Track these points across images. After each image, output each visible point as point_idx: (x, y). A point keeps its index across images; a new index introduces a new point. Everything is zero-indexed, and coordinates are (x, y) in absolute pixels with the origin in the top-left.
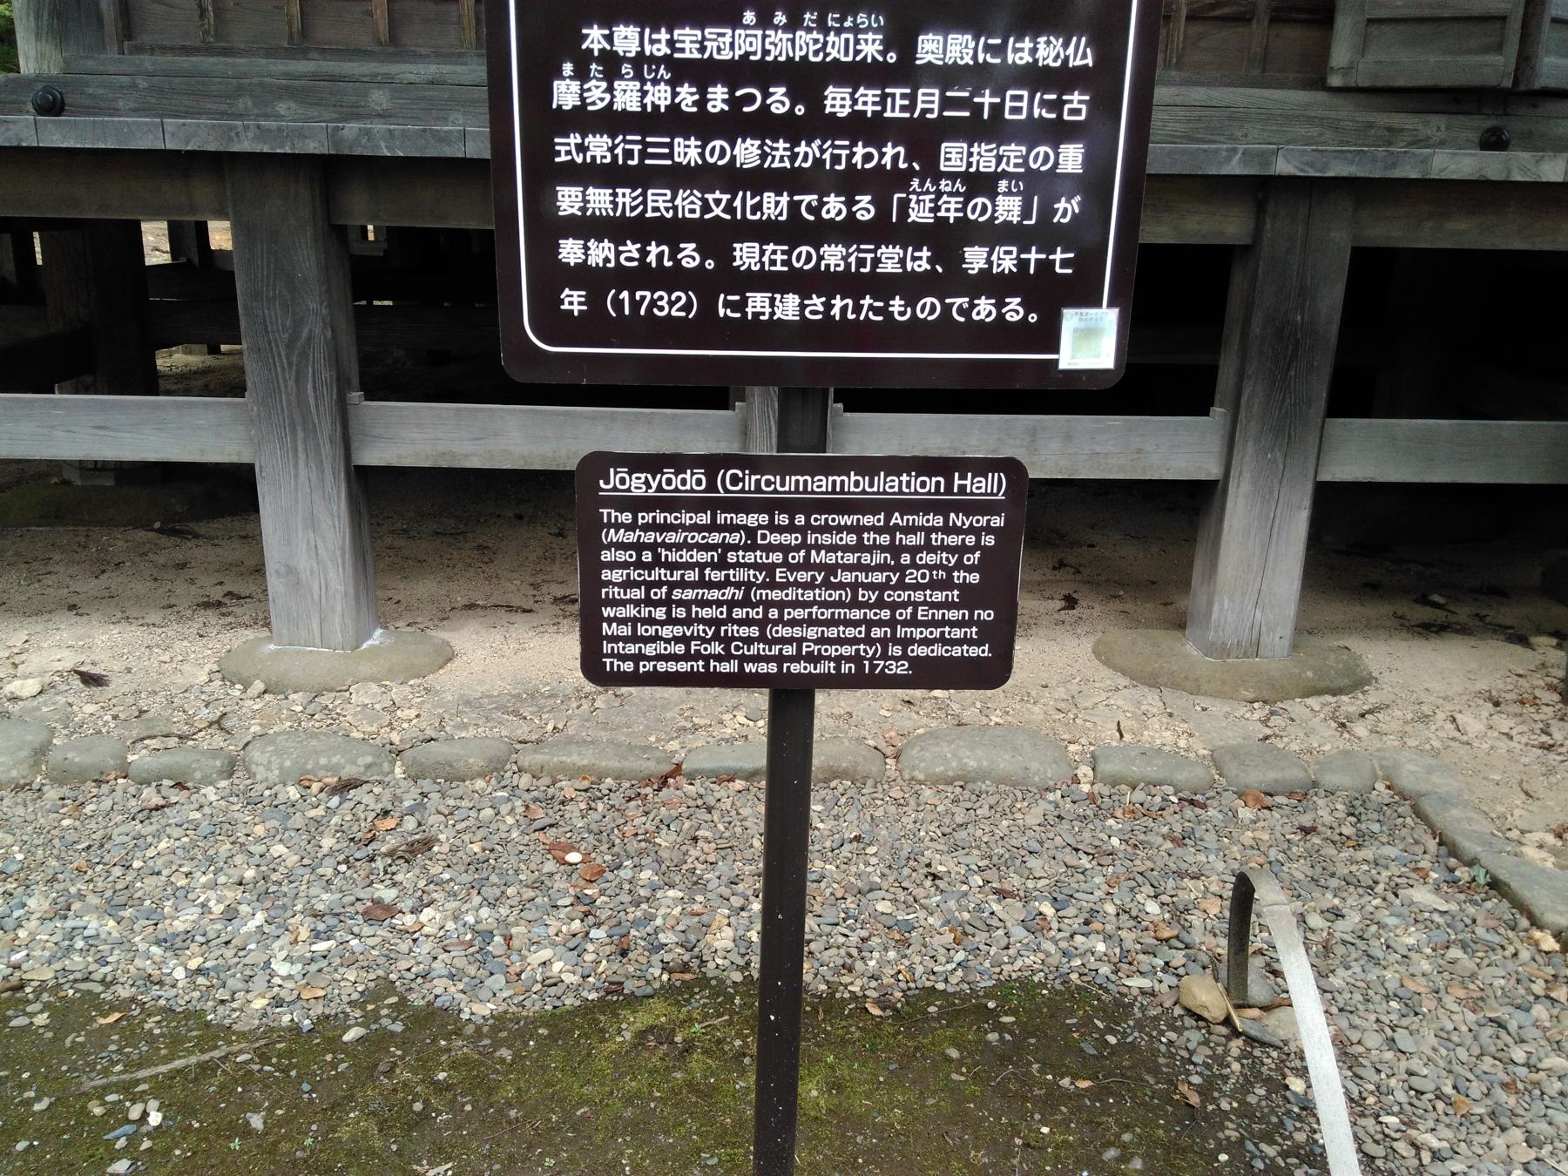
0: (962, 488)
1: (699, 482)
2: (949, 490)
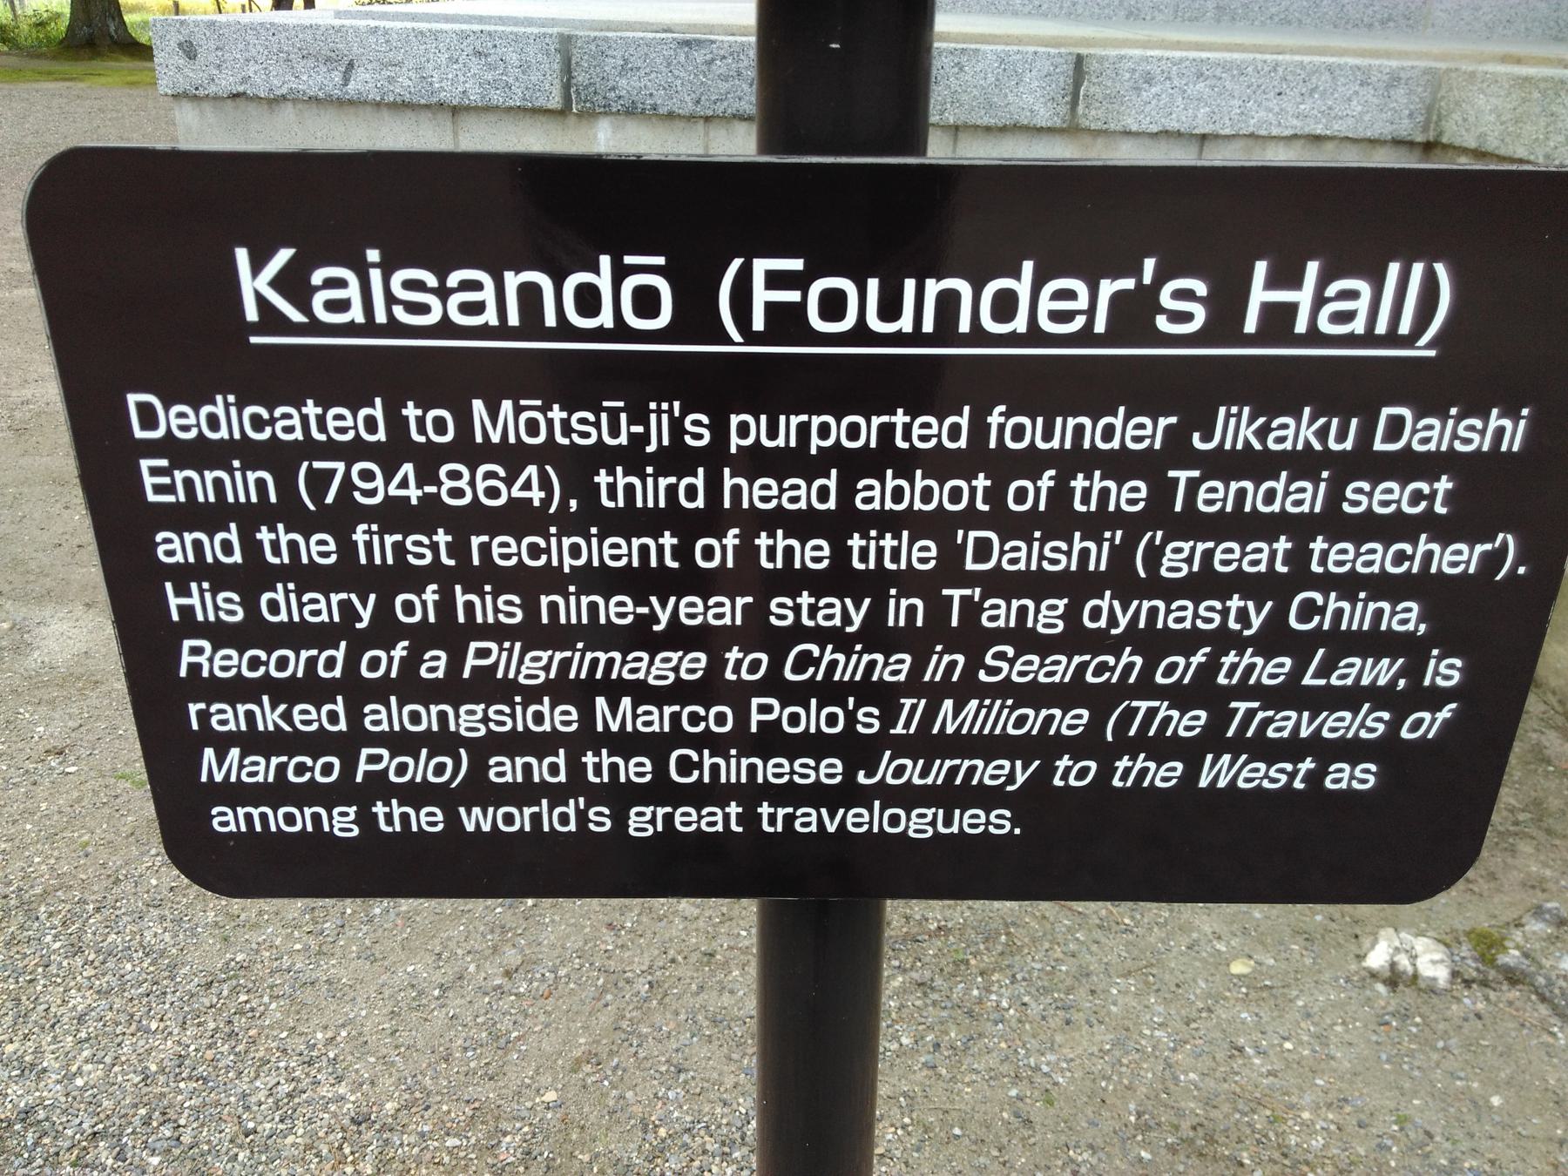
0: (1278, 320)
1: (646, 302)
2: (1225, 322)
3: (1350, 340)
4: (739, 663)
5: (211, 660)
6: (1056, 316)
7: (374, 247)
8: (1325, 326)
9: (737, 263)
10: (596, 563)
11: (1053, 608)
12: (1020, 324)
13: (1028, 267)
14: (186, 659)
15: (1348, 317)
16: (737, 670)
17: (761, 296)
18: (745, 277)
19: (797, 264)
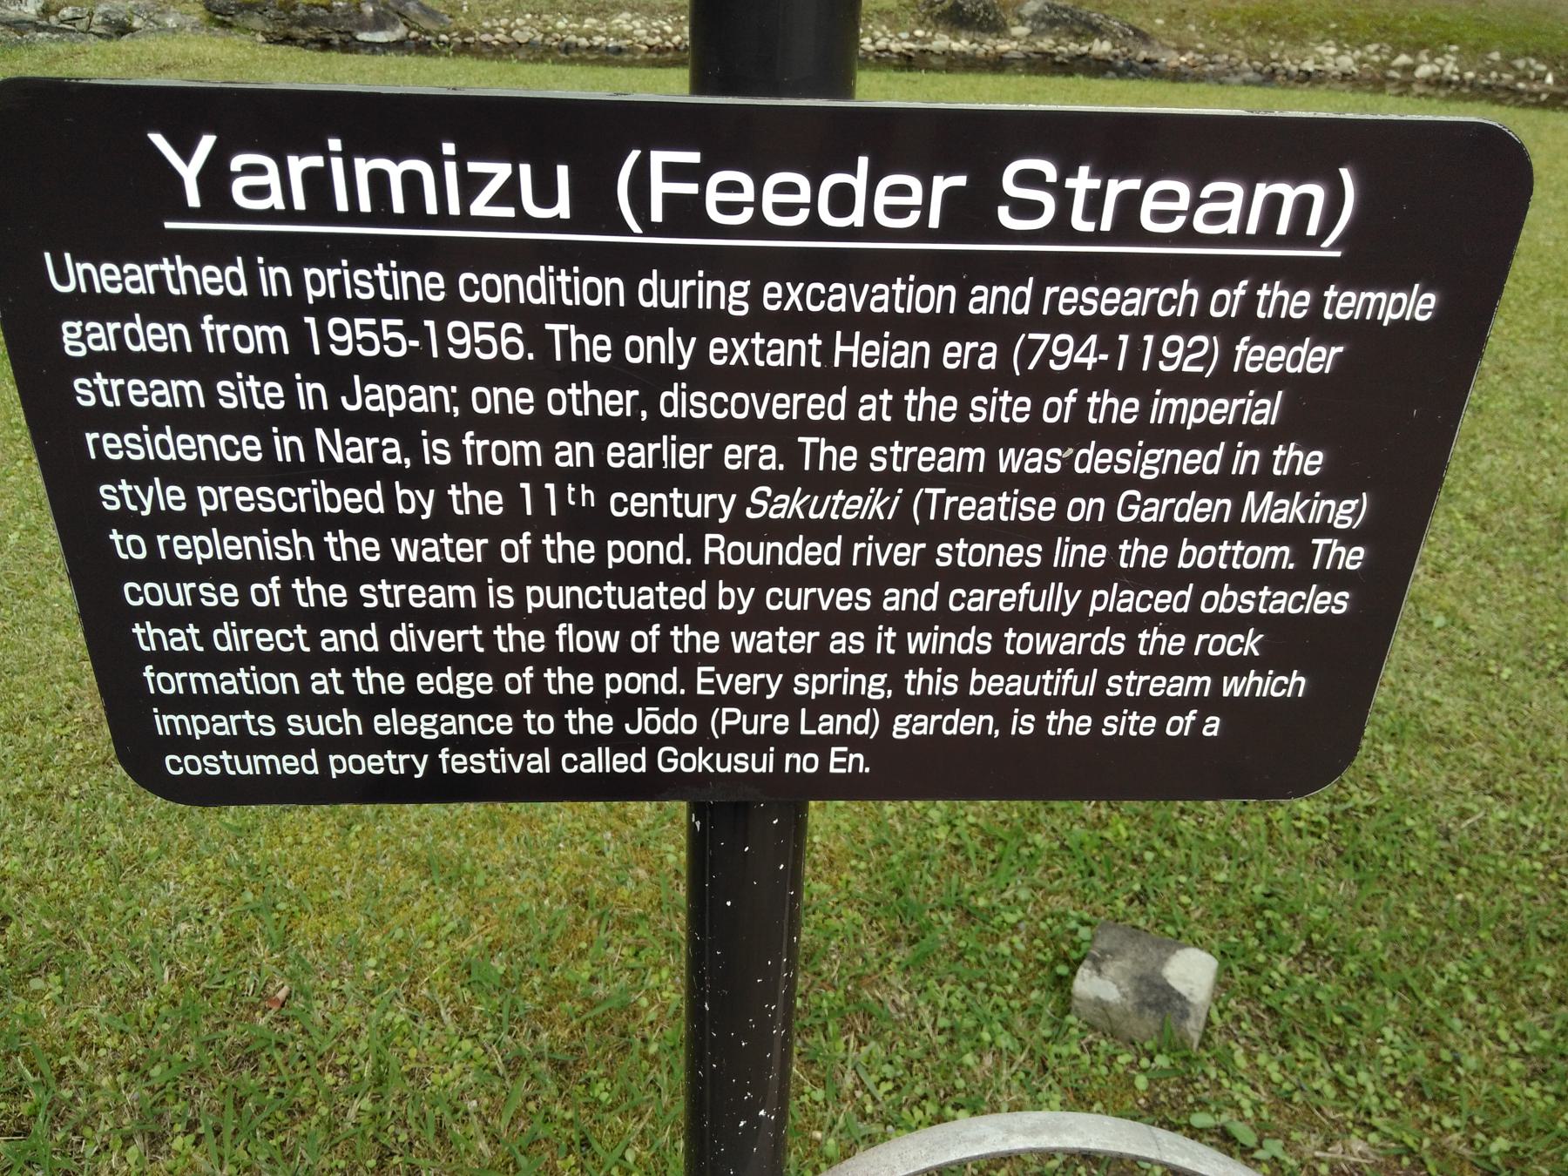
3: (1224, 240)
4: (1014, 641)
5: (725, 550)
6: (892, 211)
7: (335, 136)
8: (1200, 226)
9: (635, 155)
10: (220, 557)
11: (877, 680)
12: (857, 218)
13: (863, 163)
14: (708, 550)
15: (1223, 217)
16: (1013, 647)
17: (659, 188)
18: (642, 169)
19: (694, 157)
